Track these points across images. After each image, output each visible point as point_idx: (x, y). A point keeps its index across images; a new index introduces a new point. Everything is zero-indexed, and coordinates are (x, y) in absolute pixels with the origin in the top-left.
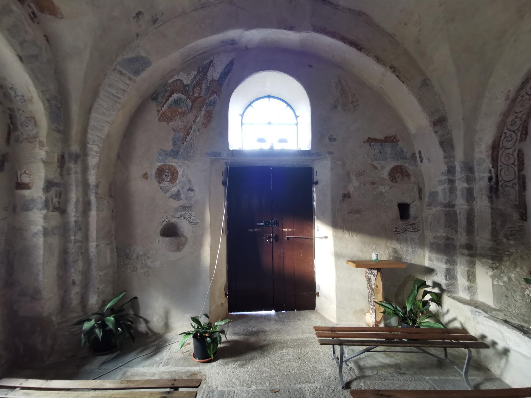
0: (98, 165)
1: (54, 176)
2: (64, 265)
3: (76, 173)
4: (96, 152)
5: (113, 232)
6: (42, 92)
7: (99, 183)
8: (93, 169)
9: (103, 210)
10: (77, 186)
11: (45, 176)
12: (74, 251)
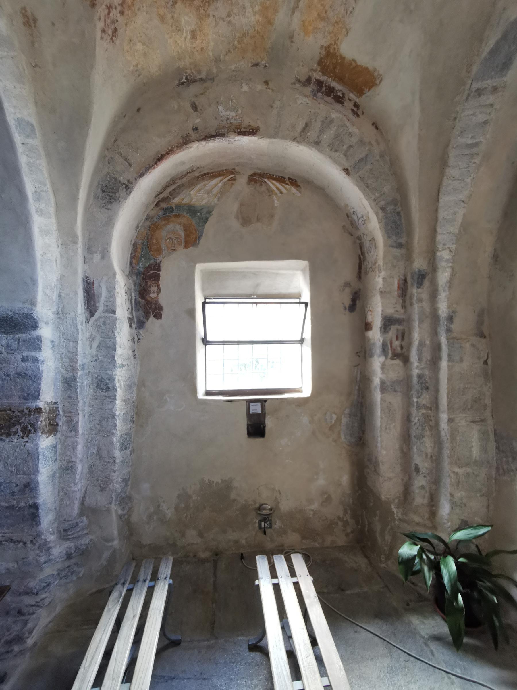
0: (450, 283)
1: (394, 309)
2: (406, 438)
3: (420, 300)
4: (447, 261)
5: (488, 401)
6: (375, 200)
7: (453, 312)
8: (444, 291)
9: (461, 360)
10: (421, 321)
11: (382, 311)
12: (416, 420)
